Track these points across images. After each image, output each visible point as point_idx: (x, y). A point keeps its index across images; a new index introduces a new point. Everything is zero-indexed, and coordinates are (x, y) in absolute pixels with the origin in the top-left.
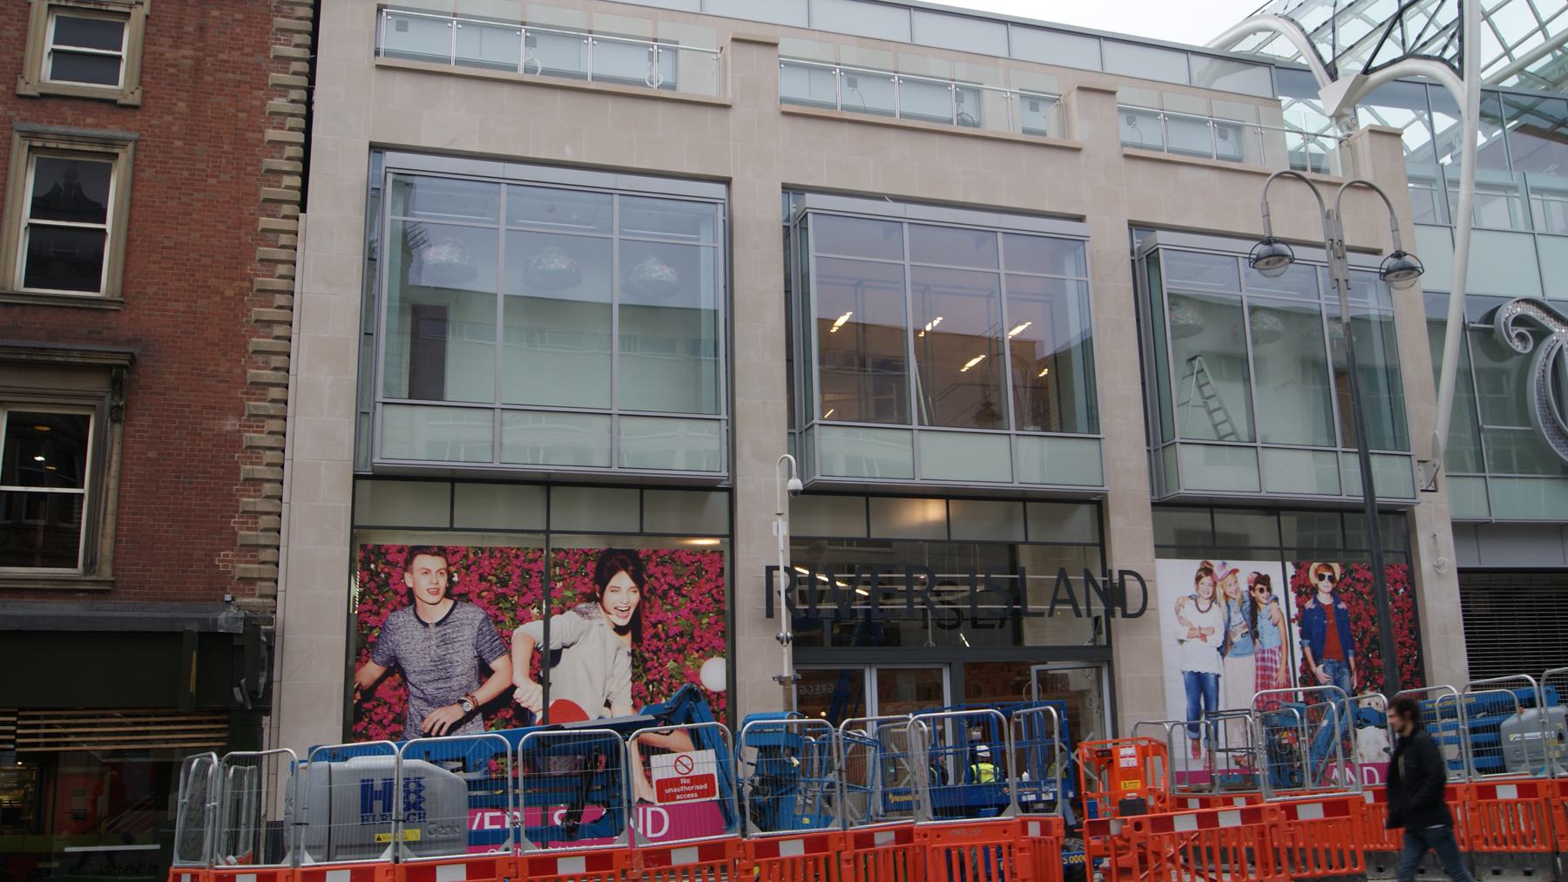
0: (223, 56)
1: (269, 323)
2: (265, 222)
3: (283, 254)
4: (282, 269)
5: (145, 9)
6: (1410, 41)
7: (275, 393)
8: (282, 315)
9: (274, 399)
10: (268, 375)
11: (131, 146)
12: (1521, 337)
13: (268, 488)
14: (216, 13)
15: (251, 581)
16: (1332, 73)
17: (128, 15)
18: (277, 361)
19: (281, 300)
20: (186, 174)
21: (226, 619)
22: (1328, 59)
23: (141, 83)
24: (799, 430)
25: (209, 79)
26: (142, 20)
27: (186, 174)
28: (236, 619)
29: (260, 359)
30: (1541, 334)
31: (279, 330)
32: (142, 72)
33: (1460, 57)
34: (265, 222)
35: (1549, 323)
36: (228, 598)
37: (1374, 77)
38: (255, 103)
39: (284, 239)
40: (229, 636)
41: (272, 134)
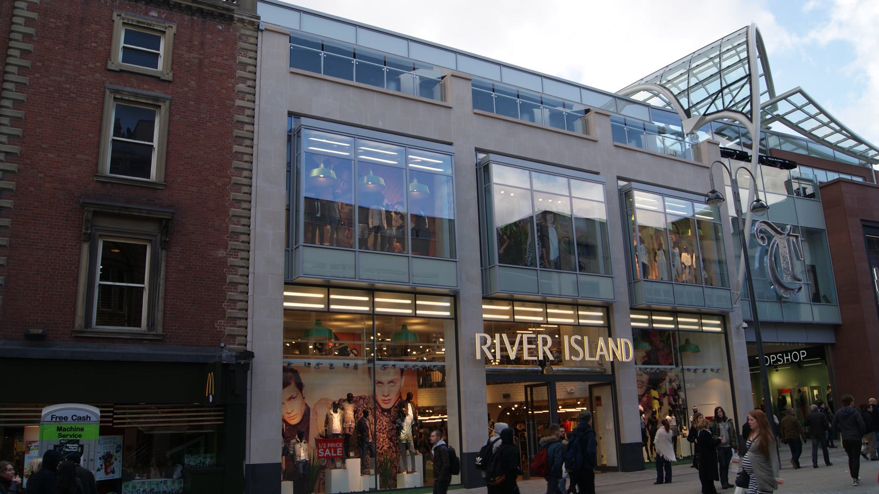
2: (236, 148)
3: (246, 166)
4: (246, 173)
5: (174, 30)
7: (243, 238)
8: (246, 197)
9: (243, 239)
11: (168, 102)
12: (762, 238)
13: (241, 288)
14: (209, 36)
15: (233, 337)
16: (688, 113)
17: (164, 32)
22: (686, 107)
23: (172, 69)
25: (207, 70)
26: (172, 36)
27: (196, 119)
28: (232, 356)
29: (235, 219)
30: (770, 238)
31: (245, 205)
32: (173, 64)
33: (751, 112)
34: (236, 148)
36: (222, 345)
37: (708, 118)
39: (246, 158)
41: (239, 103)
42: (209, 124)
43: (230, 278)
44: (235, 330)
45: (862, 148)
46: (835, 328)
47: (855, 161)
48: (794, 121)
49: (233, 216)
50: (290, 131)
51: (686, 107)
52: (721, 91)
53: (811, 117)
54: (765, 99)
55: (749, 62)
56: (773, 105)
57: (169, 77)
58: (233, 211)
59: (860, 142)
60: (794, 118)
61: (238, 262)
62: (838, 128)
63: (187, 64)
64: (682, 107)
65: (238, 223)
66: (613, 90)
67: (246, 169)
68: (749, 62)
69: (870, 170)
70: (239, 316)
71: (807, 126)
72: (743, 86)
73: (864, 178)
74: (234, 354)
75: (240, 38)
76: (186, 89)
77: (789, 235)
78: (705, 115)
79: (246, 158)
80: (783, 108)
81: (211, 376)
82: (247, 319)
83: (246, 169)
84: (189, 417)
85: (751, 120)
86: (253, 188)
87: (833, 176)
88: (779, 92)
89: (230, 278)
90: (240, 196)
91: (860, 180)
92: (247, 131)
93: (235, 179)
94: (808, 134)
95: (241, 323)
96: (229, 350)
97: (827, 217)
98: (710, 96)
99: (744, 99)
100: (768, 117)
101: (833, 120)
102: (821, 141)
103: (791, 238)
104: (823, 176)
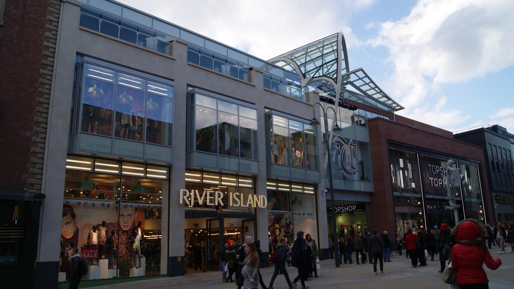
0: (31, 15)
1: (42, 103)
2: (42, 71)
3: (48, 82)
4: (47, 87)
6: (324, 73)
7: (43, 125)
10: (41, 119)
12: (338, 145)
13: (39, 155)
16: (304, 76)
18: (44, 115)
19: (46, 96)
20: (17, 51)
21: (28, 194)
22: (304, 72)
23: (4, 18)
24: (188, 152)
27: (17, 51)
29: (39, 114)
32: (4, 15)
34: (42, 71)
35: (343, 143)
36: (25, 189)
37: (315, 79)
38: (41, 32)
39: (48, 77)
40: (28, 202)
42: (26, 55)
43: (33, 149)
44: (34, 181)
45: (390, 102)
46: (371, 194)
47: (386, 109)
48: (358, 85)
49: (37, 112)
50: (77, 64)
51: (304, 72)
52: (322, 65)
53: (366, 84)
54: (344, 72)
55: (337, 52)
56: (348, 76)
57: (2, 23)
58: (38, 108)
59: (389, 99)
60: (358, 83)
61: (38, 140)
62: (379, 91)
63: (14, 16)
64: (301, 72)
65: (41, 116)
66: (266, 59)
67: (47, 84)
68: (337, 52)
69: (393, 114)
70: (37, 172)
71: (364, 88)
72: (333, 64)
73: (390, 118)
74: (33, 195)
75: (50, 5)
76: (12, 32)
77: (351, 144)
78: (313, 77)
79: (48, 77)
80: (353, 78)
81: (17, 208)
82: (42, 175)
83: (47, 84)
84: (13, 232)
85: (336, 82)
86: (51, 96)
87: (375, 116)
88: (351, 70)
89: (33, 149)
90: (42, 100)
91: (388, 118)
92: (50, 61)
93: (40, 89)
94: (364, 92)
95: (39, 177)
96: (30, 193)
97: (370, 136)
98: (316, 68)
99: (334, 71)
100: (345, 82)
101: (377, 87)
102: (370, 97)
103: (352, 146)
104: (370, 115)
